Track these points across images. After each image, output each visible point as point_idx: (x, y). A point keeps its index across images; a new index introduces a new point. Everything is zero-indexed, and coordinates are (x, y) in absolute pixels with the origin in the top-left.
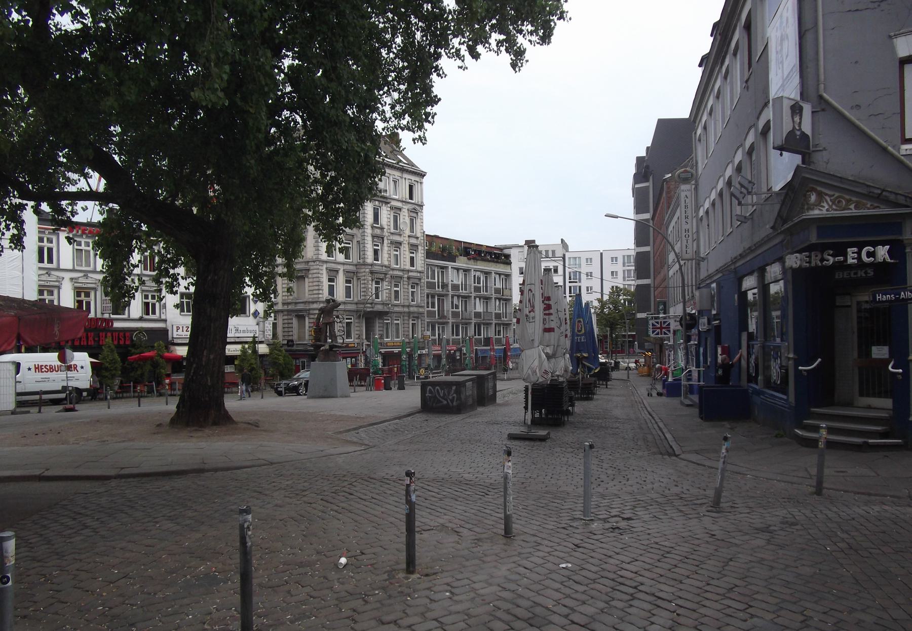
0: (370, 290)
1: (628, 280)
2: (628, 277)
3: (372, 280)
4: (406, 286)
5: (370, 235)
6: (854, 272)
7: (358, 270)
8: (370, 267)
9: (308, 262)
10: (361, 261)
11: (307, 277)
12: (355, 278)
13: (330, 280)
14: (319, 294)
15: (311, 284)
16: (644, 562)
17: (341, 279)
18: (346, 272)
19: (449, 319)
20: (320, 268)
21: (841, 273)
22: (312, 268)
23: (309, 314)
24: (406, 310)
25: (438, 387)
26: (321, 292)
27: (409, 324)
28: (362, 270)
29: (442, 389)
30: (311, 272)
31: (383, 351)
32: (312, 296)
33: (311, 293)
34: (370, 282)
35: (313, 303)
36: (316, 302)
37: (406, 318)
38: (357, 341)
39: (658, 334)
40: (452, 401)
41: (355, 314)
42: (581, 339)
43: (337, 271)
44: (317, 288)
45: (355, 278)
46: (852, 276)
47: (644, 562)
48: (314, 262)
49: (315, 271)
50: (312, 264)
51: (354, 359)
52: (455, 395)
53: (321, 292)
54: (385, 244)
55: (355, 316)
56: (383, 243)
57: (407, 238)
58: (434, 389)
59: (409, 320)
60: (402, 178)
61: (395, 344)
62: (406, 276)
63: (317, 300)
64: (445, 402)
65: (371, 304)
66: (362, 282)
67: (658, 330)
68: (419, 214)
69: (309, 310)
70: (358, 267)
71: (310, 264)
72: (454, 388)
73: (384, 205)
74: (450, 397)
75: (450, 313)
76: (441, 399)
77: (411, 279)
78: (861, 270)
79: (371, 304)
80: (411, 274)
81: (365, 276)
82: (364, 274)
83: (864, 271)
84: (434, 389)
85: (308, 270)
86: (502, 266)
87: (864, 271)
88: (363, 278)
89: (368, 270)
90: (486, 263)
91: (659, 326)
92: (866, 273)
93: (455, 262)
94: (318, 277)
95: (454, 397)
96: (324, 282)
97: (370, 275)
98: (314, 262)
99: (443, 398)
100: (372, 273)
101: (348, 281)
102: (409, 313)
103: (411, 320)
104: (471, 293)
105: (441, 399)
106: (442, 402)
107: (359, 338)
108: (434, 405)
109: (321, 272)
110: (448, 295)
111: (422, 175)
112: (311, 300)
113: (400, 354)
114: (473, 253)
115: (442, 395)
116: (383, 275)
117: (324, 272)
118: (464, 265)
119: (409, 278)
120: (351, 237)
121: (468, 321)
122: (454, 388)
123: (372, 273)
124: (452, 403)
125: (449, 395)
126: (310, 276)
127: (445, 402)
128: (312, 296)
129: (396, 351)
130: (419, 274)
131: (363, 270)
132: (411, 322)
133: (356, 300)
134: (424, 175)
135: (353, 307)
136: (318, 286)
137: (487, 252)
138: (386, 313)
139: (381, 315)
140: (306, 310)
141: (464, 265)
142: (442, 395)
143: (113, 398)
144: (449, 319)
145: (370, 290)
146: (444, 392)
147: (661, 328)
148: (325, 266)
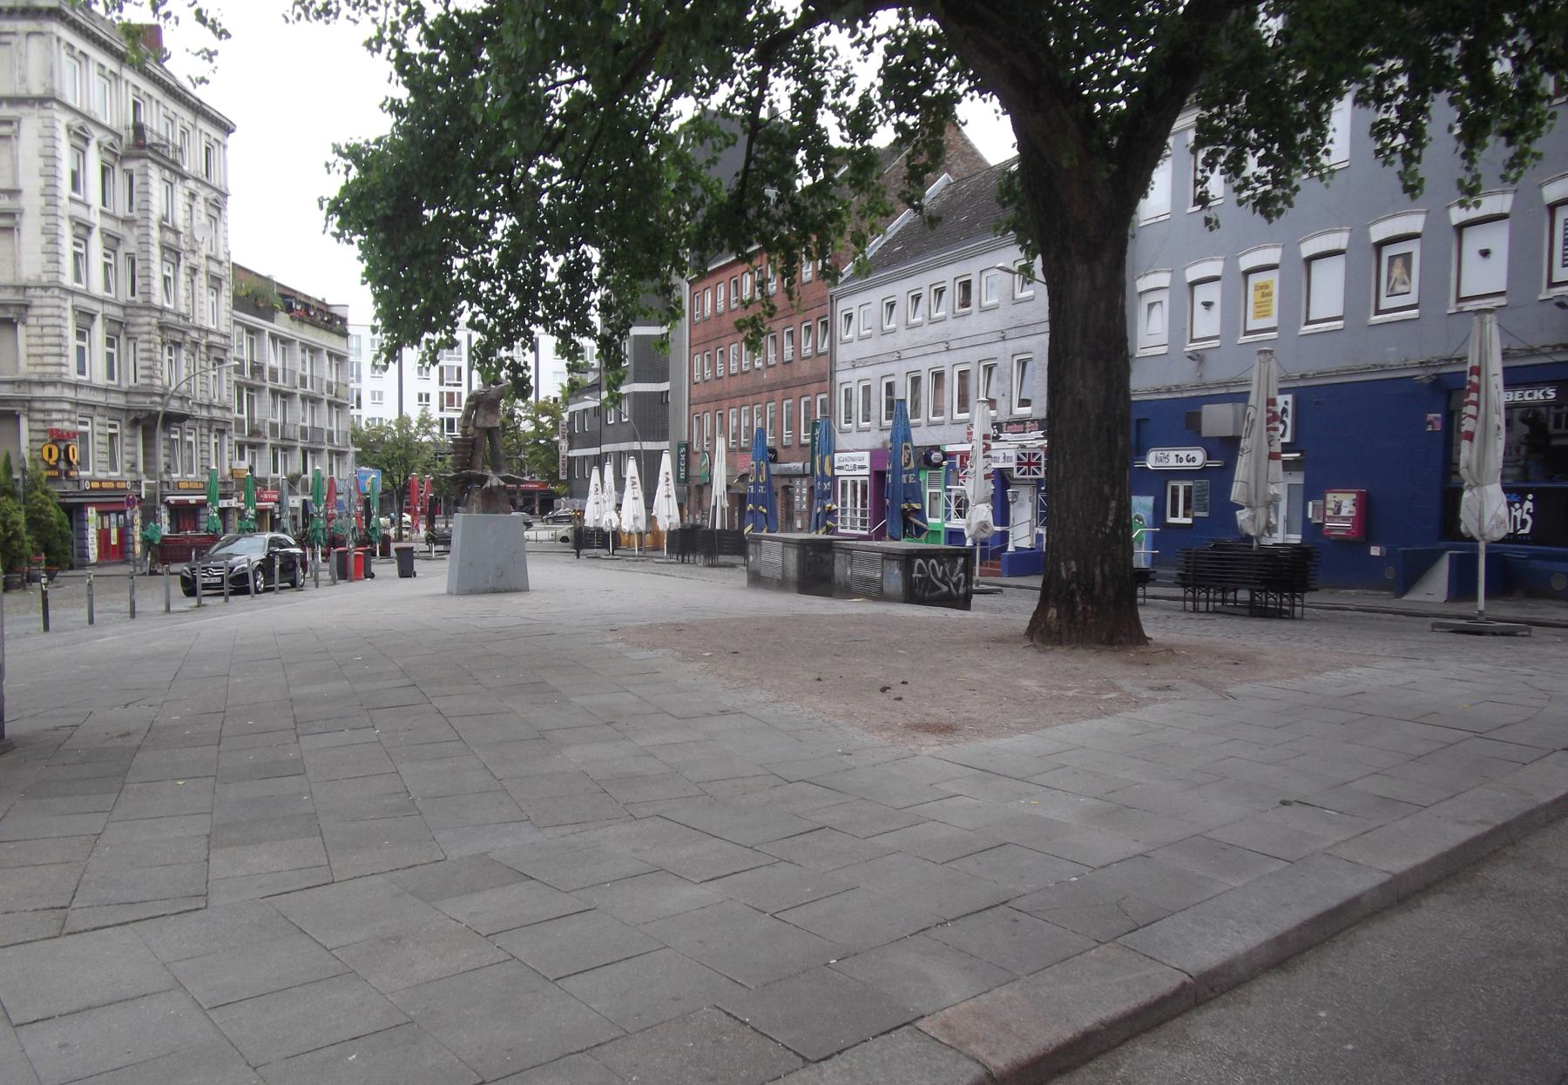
0: (159, 364)
1: (447, 384)
2: (448, 379)
3: (163, 344)
4: (204, 364)
5: (157, 244)
6: (1528, 392)
7: (132, 320)
8: (158, 314)
9: (25, 288)
10: (139, 299)
11: (24, 323)
12: (122, 337)
13: (80, 335)
14: (61, 365)
15: (33, 340)
16: (287, 893)
17: (99, 331)
18: (109, 320)
19: (266, 438)
20: (62, 304)
21: (1511, 393)
22: (36, 302)
23: (30, 410)
24: (204, 413)
25: (933, 561)
26: (64, 360)
27: (208, 444)
28: (141, 320)
29: (940, 564)
30: (36, 311)
31: (172, 499)
32: (40, 369)
33: (33, 360)
34: (159, 347)
35: (42, 384)
36: (54, 384)
37: (205, 431)
38: (127, 476)
39: (1024, 474)
40: (957, 586)
41: (122, 416)
42: (908, 479)
43: (92, 317)
44: (56, 350)
45: (122, 337)
46: (1527, 398)
47: (287, 893)
48: (45, 288)
49: (48, 311)
50: (39, 292)
51: (121, 517)
52: (962, 575)
53: (64, 360)
54: (182, 268)
55: (124, 421)
56: (178, 265)
57: (203, 261)
58: (927, 564)
59: (209, 436)
60: (194, 127)
61: (191, 485)
62: (204, 342)
63: (55, 378)
64: (945, 589)
65: (162, 396)
66: (140, 346)
67: (1026, 467)
68: (222, 212)
69: (30, 400)
70: (129, 311)
71: (31, 292)
72: (961, 561)
73: (178, 181)
74: (955, 579)
75: (299, 429)
76: (937, 583)
77: (213, 350)
78: (1539, 390)
79: (162, 396)
80: (212, 338)
81: (149, 333)
82: (146, 329)
83: (1542, 391)
84: (927, 564)
85: (27, 307)
86: (335, 338)
87: (1542, 391)
88: (146, 337)
89: (154, 321)
90: (316, 331)
91: (1026, 460)
92: (1545, 394)
93: (273, 322)
94: (60, 326)
95: (960, 579)
96: (70, 338)
97: (158, 332)
98: (45, 288)
99: (942, 581)
100: (163, 327)
101: (110, 343)
102: (211, 421)
103: (213, 435)
104: (296, 388)
105: (937, 583)
106: (940, 589)
107: (130, 471)
108: (926, 594)
109: (64, 314)
110: (263, 387)
111: (226, 128)
112: (35, 377)
113: (202, 504)
114: (299, 307)
115: (940, 575)
116: (180, 336)
117: (69, 314)
118: (287, 331)
119: (209, 346)
120: (114, 241)
121: (290, 443)
122: (961, 561)
123: (163, 327)
124: (957, 590)
125: (952, 575)
126: (31, 321)
127: (945, 589)
128: (40, 369)
129: (192, 499)
130: (223, 341)
131: (147, 319)
132: (213, 440)
133: (124, 386)
134: (233, 131)
135: (116, 400)
136: (60, 345)
137: (318, 309)
138: (181, 418)
139: (172, 419)
140: (23, 401)
141: (287, 331)
142: (940, 575)
143: (232, 594)
144: (266, 438)
145: (159, 364)
146: (944, 570)
147: (1029, 464)
148: (69, 305)
